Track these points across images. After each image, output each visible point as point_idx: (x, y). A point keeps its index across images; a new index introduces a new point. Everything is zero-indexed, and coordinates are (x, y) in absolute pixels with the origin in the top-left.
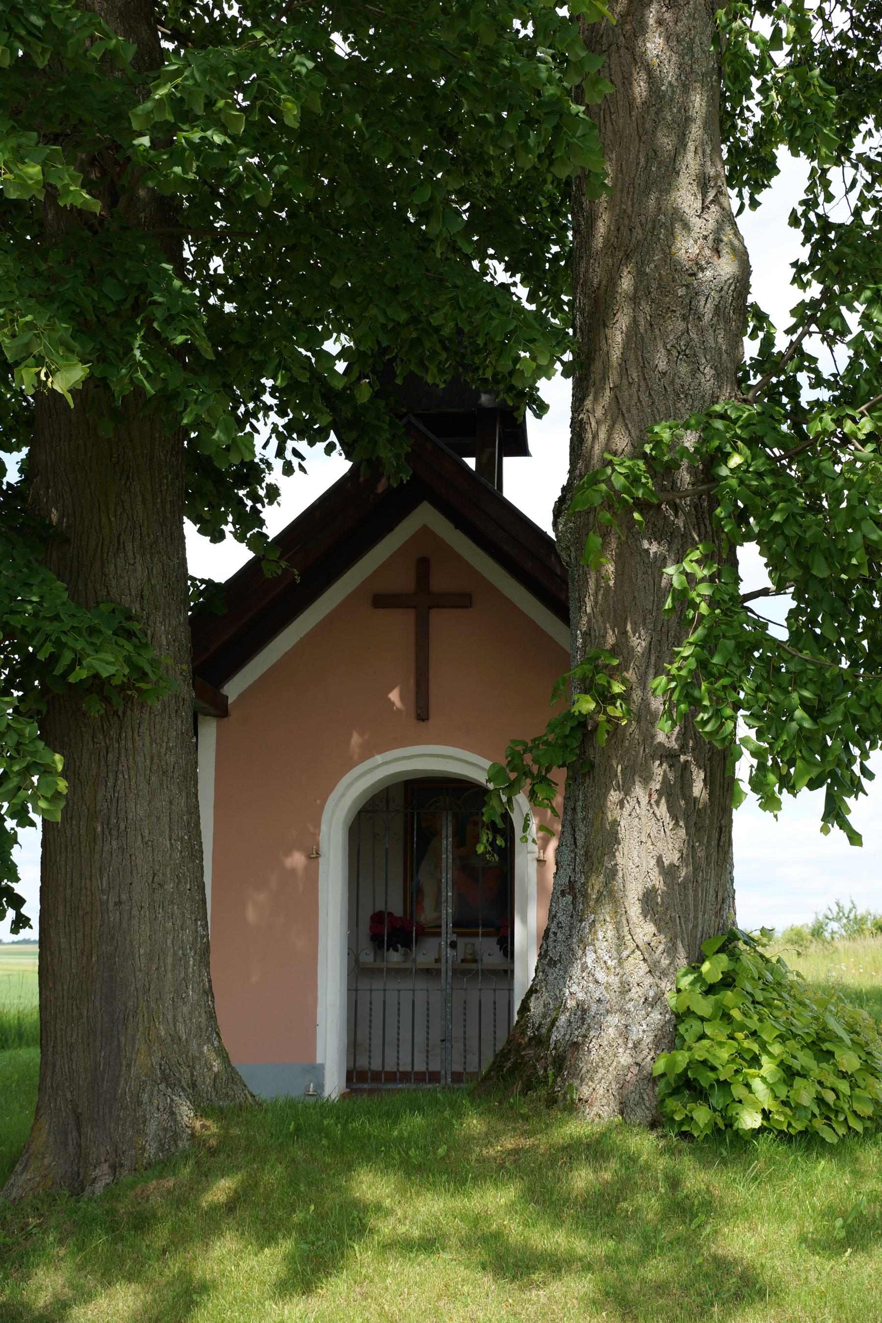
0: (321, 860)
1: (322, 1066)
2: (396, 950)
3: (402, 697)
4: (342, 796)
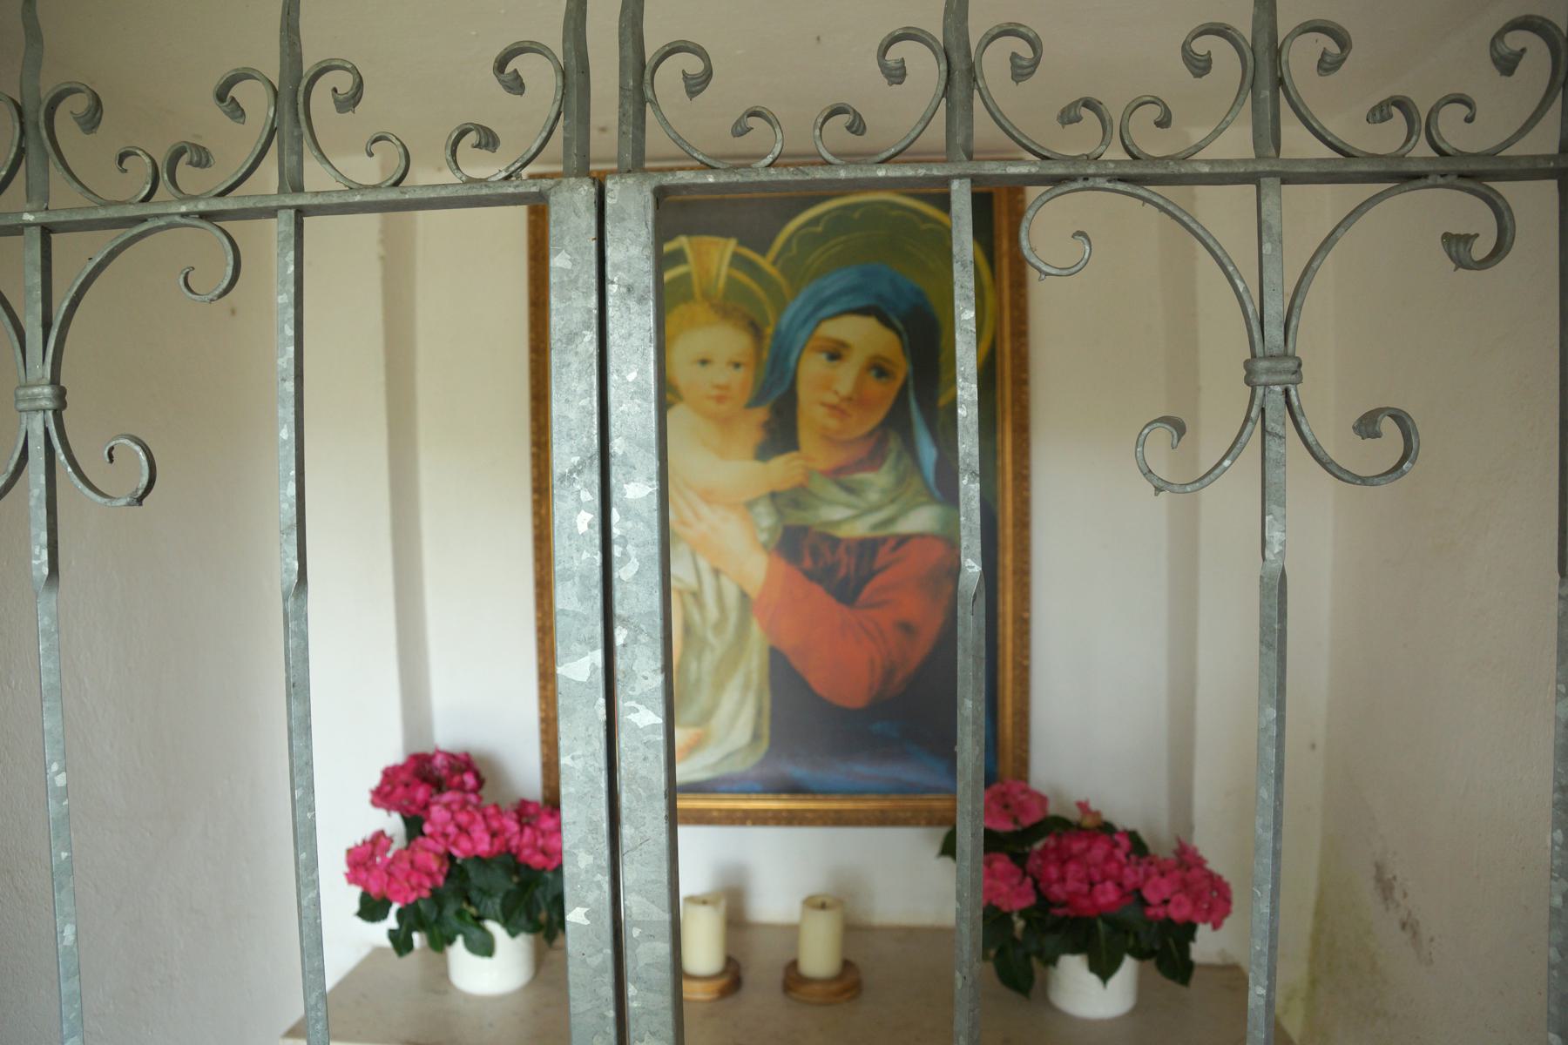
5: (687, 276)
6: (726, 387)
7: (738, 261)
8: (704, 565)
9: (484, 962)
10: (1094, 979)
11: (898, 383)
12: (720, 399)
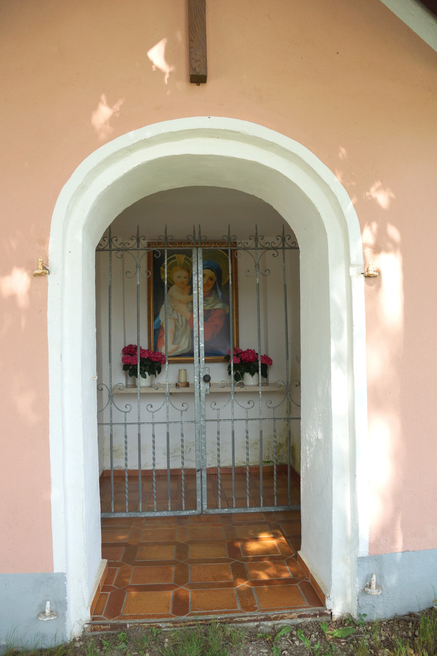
0: (50, 278)
1: (62, 577)
2: (145, 377)
3: (169, 57)
4: (82, 188)
5: (176, 261)
6: (183, 282)
7: (186, 259)
8: (179, 314)
9: (144, 379)
10: (251, 376)
11: (214, 282)
12: (182, 284)
